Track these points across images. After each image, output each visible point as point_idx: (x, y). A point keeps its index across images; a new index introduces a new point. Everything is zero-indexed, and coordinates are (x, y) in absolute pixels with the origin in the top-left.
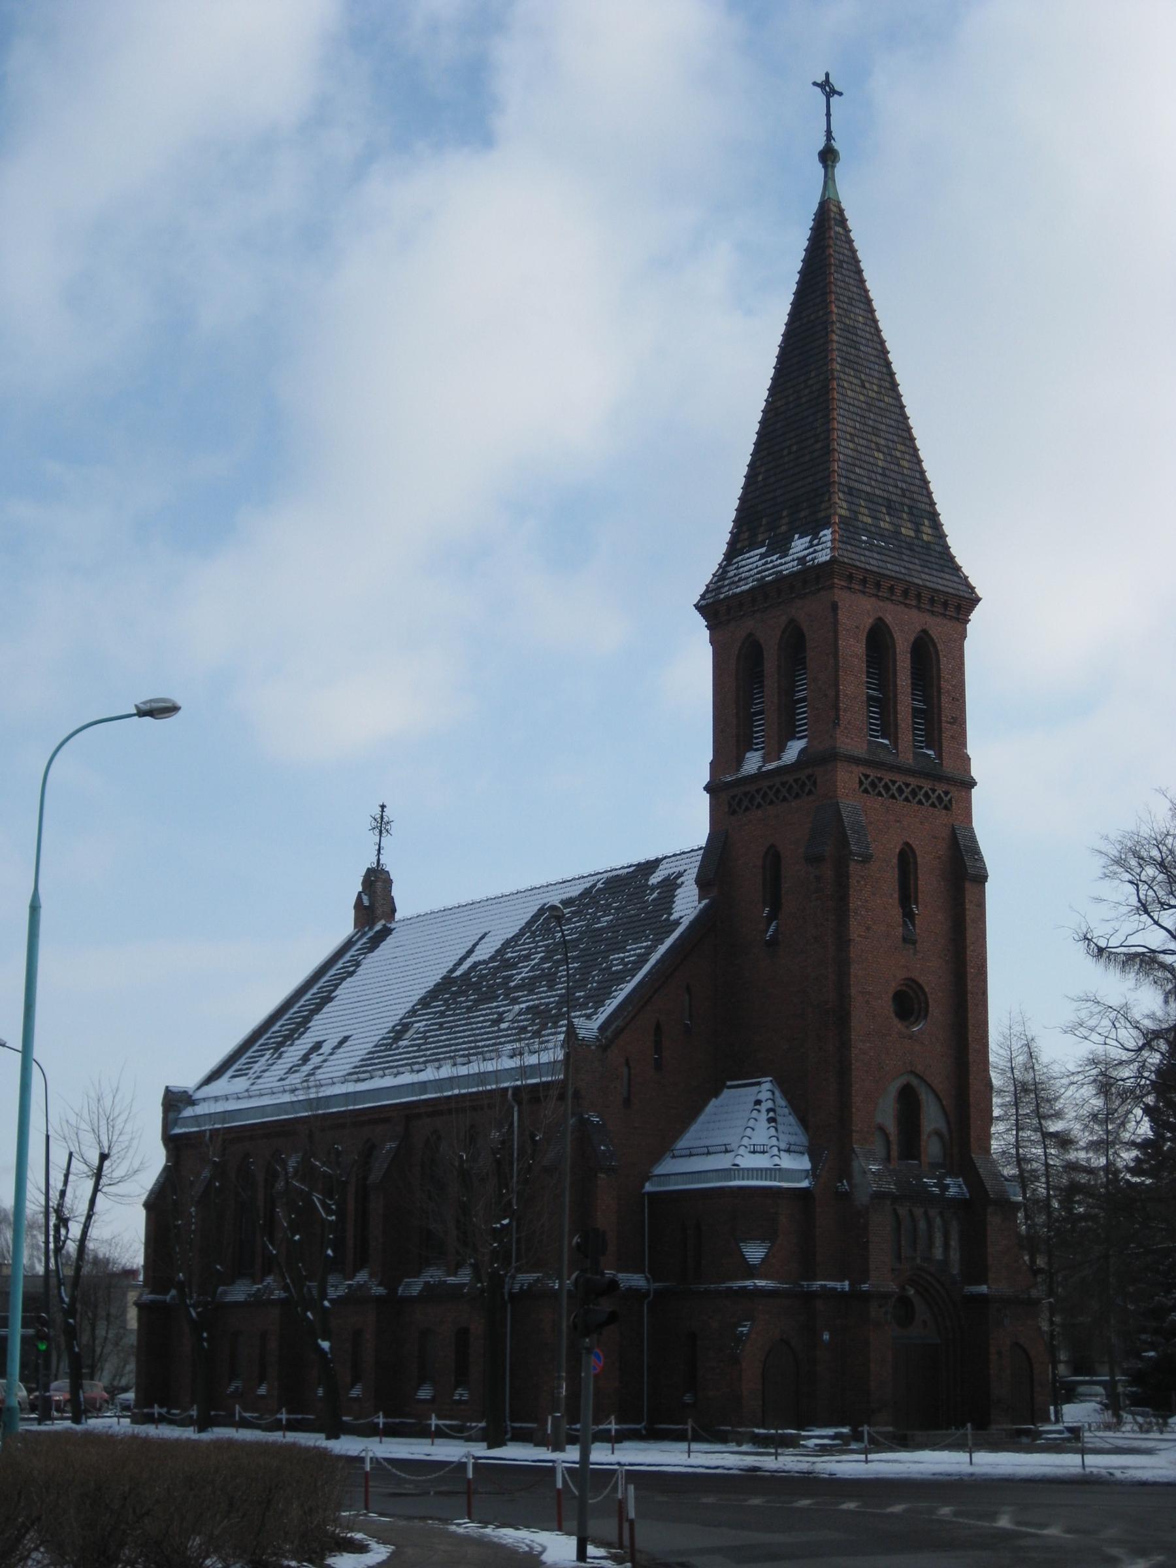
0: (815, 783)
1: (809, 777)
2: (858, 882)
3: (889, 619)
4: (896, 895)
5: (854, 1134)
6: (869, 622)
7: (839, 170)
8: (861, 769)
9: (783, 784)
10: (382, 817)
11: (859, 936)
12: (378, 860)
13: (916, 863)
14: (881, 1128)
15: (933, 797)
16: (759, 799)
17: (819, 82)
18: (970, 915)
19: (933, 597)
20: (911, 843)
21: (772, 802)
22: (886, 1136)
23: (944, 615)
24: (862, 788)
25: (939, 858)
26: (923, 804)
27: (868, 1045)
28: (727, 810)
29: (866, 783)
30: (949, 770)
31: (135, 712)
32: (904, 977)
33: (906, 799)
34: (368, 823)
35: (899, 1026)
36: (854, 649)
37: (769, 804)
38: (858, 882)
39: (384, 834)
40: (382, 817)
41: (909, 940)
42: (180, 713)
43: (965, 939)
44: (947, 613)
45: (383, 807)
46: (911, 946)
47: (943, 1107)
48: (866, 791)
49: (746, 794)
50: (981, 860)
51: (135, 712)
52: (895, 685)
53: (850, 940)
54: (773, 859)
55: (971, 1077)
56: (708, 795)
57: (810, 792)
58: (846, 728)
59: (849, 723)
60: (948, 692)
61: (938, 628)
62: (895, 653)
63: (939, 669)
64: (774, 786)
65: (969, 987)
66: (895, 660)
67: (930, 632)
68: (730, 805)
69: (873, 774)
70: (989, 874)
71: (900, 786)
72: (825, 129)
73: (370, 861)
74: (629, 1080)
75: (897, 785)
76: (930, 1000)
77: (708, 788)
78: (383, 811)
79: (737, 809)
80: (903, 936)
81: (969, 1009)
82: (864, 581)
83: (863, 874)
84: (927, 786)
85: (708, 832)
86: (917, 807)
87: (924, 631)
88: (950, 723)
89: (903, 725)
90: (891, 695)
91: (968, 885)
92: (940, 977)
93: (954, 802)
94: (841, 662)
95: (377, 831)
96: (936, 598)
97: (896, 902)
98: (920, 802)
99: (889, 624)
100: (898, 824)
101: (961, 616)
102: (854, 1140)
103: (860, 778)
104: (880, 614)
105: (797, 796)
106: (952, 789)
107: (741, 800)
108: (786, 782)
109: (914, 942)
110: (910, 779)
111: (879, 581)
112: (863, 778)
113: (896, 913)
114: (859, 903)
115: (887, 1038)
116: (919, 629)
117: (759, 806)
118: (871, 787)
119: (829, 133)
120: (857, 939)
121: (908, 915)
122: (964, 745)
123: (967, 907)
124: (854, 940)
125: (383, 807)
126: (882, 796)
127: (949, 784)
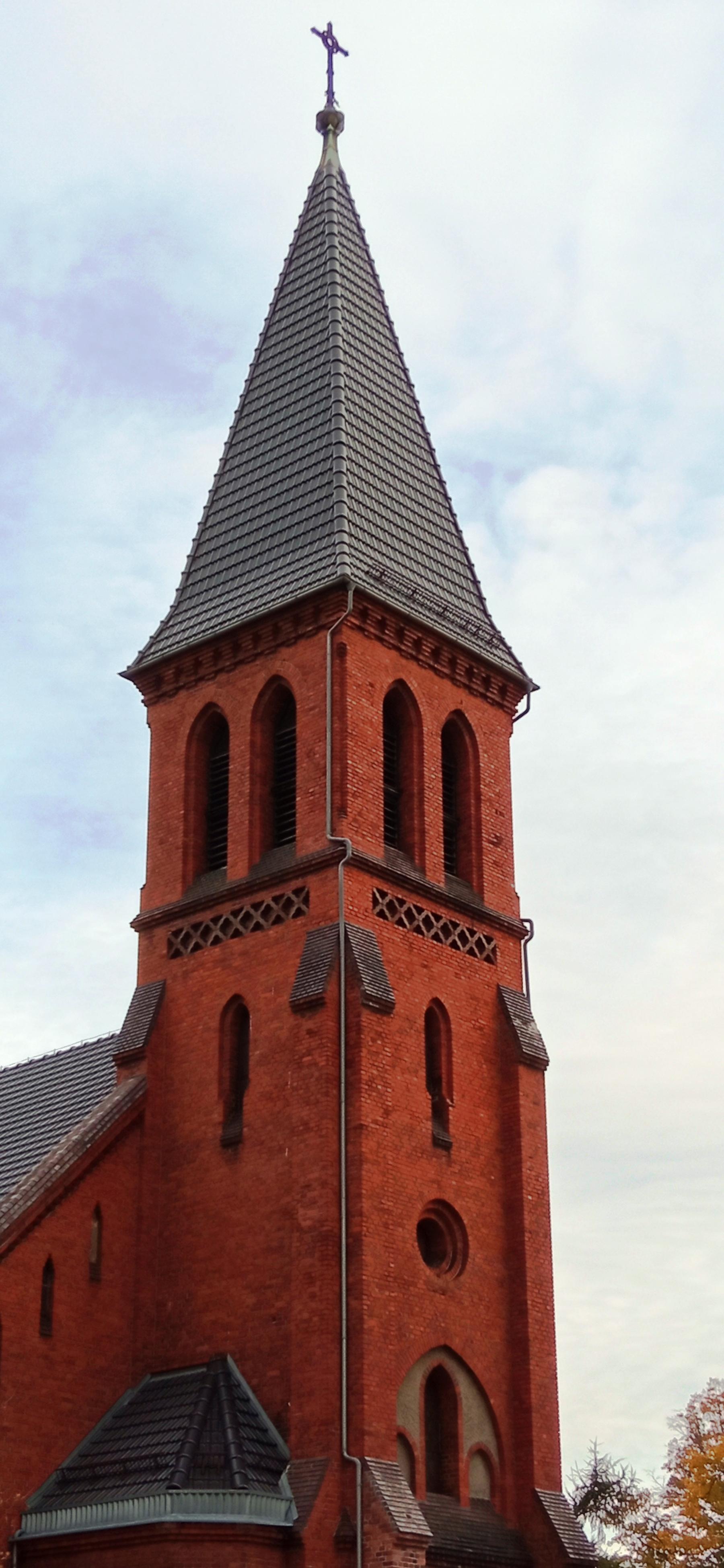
0: (306, 901)
1: (297, 892)
3: (413, 685)
4: (423, 1073)
5: (366, 1438)
6: (385, 682)
8: (376, 882)
9: (256, 906)
11: (375, 1122)
13: (449, 1031)
14: (402, 1438)
15: (473, 940)
16: (217, 932)
17: (321, 31)
18: (526, 1115)
19: (471, 667)
20: (442, 1000)
21: (237, 934)
23: (484, 697)
24: (378, 909)
25: (481, 1029)
26: (458, 948)
27: (387, 1293)
28: (165, 952)
30: (492, 907)
32: (433, 1197)
33: (436, 937)
35: (428, 1271)
37: (233, 937)
41: (442, 1144)
43: (518, 1149)
46: (444, 1153)
48: (381, 914)
49: (196, 927)
52: (421, 776)
53: (362, 1125)
55: (532, 1362)
57: (299, 913)
58: (355, 820)
59: (360, 814)
60: (490, 800)
62: (421, 733)
63: (477, 768)
64: (241, 909)
65: (527, 1222)
66: (421, 742)
67: (466, 715)
68: (170, 944)
69: (394, 893)
70: (551, 1059)
71: (427, 917)
72: (326, 88)
75: (424, 915)
76: (470, 1238)
79: (182, 949)
80: (433, 1135)
81: (527, 1256)
82: (382, 625)
83: (381, 1030)
84: (464, 925)
85: (135, 986)
88: (492, 843)
89: (431, 833)
90: (416, 790)
91: (522, 1070)
92: (483, 1205)
93: (498, 954)
94: (350, 727)
96: (475, 670)
97: (423, 1083)
98: (454, 945)
99: (414, 692)
100: (425, 970)
101: (506, 703)
102: (366, 1448)
103: (374, 894)
105: (278, 920)
106: (496, 934)
110: (441, 910)
113: (423, 1101)
114: (375, 1072)
115: (412, 1288)
116: (452, 708)
119: (330, 93)
120: (373, 1125)
121: (439, 1113)
123: (522, 1102)
124: (367, 1126)
126: (404, 926)
127: (492, 927)
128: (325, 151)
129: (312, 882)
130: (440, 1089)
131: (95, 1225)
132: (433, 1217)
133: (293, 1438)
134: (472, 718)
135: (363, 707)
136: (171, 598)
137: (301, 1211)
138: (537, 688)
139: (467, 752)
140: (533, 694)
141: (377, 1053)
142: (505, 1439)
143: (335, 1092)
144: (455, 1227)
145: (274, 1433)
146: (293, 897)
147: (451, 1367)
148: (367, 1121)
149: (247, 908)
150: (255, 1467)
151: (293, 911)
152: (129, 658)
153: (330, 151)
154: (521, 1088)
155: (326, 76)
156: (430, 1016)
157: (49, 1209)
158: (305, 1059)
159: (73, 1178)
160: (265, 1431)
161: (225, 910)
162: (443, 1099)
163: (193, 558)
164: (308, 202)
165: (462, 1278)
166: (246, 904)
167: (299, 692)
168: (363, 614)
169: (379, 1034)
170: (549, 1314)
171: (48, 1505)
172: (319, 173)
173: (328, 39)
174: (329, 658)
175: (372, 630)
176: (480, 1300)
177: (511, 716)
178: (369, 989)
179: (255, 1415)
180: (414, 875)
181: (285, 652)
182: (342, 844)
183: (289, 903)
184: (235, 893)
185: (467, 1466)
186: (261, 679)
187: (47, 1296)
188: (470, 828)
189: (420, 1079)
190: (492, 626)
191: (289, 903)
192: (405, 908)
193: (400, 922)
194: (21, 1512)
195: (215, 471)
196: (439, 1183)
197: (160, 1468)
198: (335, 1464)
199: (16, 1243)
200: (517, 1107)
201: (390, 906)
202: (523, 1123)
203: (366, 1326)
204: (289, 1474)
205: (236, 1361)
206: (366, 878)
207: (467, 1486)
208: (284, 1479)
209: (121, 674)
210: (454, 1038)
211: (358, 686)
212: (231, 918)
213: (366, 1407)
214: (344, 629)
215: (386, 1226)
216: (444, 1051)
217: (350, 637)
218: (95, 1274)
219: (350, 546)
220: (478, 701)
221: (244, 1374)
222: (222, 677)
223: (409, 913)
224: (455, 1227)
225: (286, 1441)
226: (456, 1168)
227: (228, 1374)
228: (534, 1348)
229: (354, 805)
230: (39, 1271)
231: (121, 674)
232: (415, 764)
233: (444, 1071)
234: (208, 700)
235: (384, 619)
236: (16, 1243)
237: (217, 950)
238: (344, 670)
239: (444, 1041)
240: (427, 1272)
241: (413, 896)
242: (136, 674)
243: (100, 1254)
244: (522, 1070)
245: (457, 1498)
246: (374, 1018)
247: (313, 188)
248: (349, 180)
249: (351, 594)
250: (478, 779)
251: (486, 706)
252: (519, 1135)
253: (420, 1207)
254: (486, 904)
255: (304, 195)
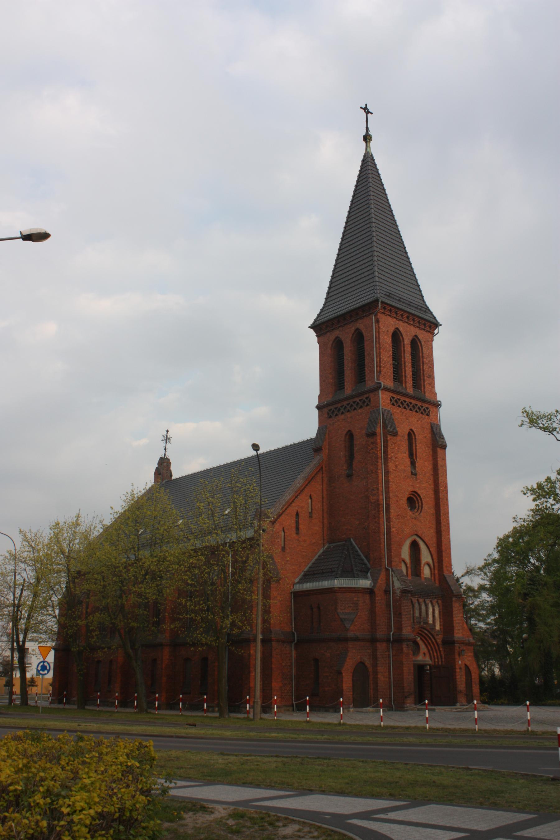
0: (370, 401)
1: (367, 398)
2: (392, 445)
3: (401, 329)
4: (407, 453)
6: (392, 330)
7: (372, 143)
8: (391, 394)
9: (354, 402)
10: (167, 436)
12: (165, 454)
14: (404, 561)
15: (422, 409)
16: (342, 410)
17: (363, 107)
21: (348, 411)
22: (406, 564)
24: (392, 403)
25: (425, 437)
28: (327, 416)
29: (393, 401)
30: (428, 398)
31: (20, 236)
32: (411, 490)
33: (411, 410)
34: (162, 438)
35: (410, 513)
36: (387, 340)
38: (392, 445)
39: (168, 443)
40: (167, 436)
42: (49, 239)
43: (438, 474)
44: (425, 329)
45: (167, 431)
47: (430, 552)
48: (393, 404)
49: (336, 408)
50: (443, 438)
51: (20, 236)
54: (350, 435)
55: (443, 538)
56: (317, 411)
57: (367, 405)
61: (422, 335)
66: (404, 347)
68: (328, 414)
69: (397, 397)
73: (161, 454)
74: (284, 538)
77: (317, 407)
78: (167, 433)
79: (332, 415)
84: (419, 404)
86: (415, 413)
87: (416, 336)
95: (165, 442)
98: (416, 411)
101: (431, 331)
104: (397, 326)
105: (361, 407)
106: (430, 406)
107: (333, 411)
108: (356, 402)
109: (415, 475)
111: (397, 312)
112: (392, 399)
113: (408, 461)
116: (414, 334)
117: (342, 413)
118: (395, 402)
119: (367, 128)
121: (413, 464)
122: (434, 387)
125: (167, 431)
128: (366, 149)
129: (371, 395)
130: (413, 457)
131: (310, 501)
132: (412, 496)
133: (371, 563)
134: (420, 337)
135: (385, 339)
136: (323, 301)
137: (371, 497)
138: (441, 325)
139: (419, 348)
140: (440, 327)
141: (393, 449)
142: (435, 560)
143: (380, 461)
144: (419, 498)
145: (366, 561)
146: (366, 400)
147: (418, 540)
148: (391, 470)
149: (352, 403)
150: (361, 571)
151: (365, 404)
152: (311, 322)
153: (368, 148)
154: (438, 455)
155: (365, 122)
156: (410, 435)
157: (296, 497)
158: (371, 451)
159: (302, 488)
160: (363, 560)
161: (345, 403)
162: (414, 460)
163: (330, 288)
164: (361, 166)
165: (421, 514)
166: (351, 401)
167: (364, 334)
168: (384, 308)
169: (394, 443)
170: (448, 523)
171: (302, 581)
172: (365, 156)
173: (366, 110)
174: (374, 323)
175: (387, 313)
176: (427, 520)
177: (433, 334)
178: (389, 429)
179: (360, 556)
180: (403, 391)
181: (360, 321)
182: (380, 383)
183: (364, 402)
184: (347, 399)
185: (423, 567)
186: (353, 329)
187: (297, 522)
188: (420, 373)
189: (406, 455)
190: (426, 305)
191: (364, 402)
192: (400, 401)
193: (399, 406)
194: (294, 584)
195: (335, 259)
196: (413, 486)
197: (332, 572)
198: (384, 570)
199: (287, 508)
200: (437, 461)
201: (396, 401)
202: (439, 466)
203: (392, 531)
204: (371, 573)
205: (354, 540)
206: (388, 393)
207: (423, 574)
208: (369, 574)
209: (309, 327)
210: (417, 440)
211: (384, 332)
212: (347, 406)
213: (392, 554)
214: (378, 314)
215: (397, 501)
216: (414, 445)
217: (380, 316)
218: (311, 515)
219: (379, 286)
220: (423, 332)
221: (356, 544)
222: (340, 329)
223: (402, 403)
224: (419, 498)
225: (369, 563)
226: (419, 481)
227: (352, 544)
228: (443, 533)
229: (384, 371)
230: (294, 516)
231: (309, 327)
232: (402, 355)
233: (414, 451)
234: (336, 336)
235: (391, 309)
236: (287, 508)
237: (343, 416)
238: (379, 327)
239: (414, 442)
240: (410, 513)
241: (403, 397)
242: (313, 327)
243: (312, 509)
244: (438, 449)
245: (420, 577)
246: (392, 437)
247: (363, 161)
248: (375, 158)
249: (380, 303)
250: (423, 357)
251: (425, 333)
252: (438, 470)
253: (407, 493)
254: (426, 397)
255: (360, 163)
